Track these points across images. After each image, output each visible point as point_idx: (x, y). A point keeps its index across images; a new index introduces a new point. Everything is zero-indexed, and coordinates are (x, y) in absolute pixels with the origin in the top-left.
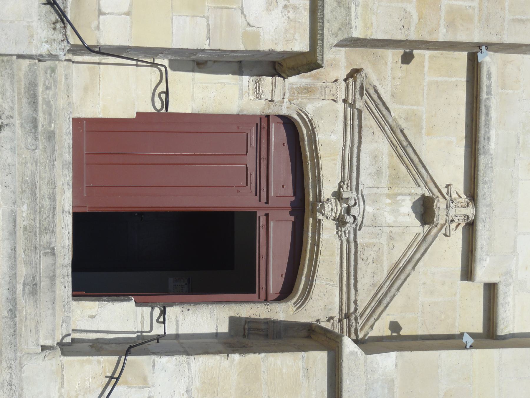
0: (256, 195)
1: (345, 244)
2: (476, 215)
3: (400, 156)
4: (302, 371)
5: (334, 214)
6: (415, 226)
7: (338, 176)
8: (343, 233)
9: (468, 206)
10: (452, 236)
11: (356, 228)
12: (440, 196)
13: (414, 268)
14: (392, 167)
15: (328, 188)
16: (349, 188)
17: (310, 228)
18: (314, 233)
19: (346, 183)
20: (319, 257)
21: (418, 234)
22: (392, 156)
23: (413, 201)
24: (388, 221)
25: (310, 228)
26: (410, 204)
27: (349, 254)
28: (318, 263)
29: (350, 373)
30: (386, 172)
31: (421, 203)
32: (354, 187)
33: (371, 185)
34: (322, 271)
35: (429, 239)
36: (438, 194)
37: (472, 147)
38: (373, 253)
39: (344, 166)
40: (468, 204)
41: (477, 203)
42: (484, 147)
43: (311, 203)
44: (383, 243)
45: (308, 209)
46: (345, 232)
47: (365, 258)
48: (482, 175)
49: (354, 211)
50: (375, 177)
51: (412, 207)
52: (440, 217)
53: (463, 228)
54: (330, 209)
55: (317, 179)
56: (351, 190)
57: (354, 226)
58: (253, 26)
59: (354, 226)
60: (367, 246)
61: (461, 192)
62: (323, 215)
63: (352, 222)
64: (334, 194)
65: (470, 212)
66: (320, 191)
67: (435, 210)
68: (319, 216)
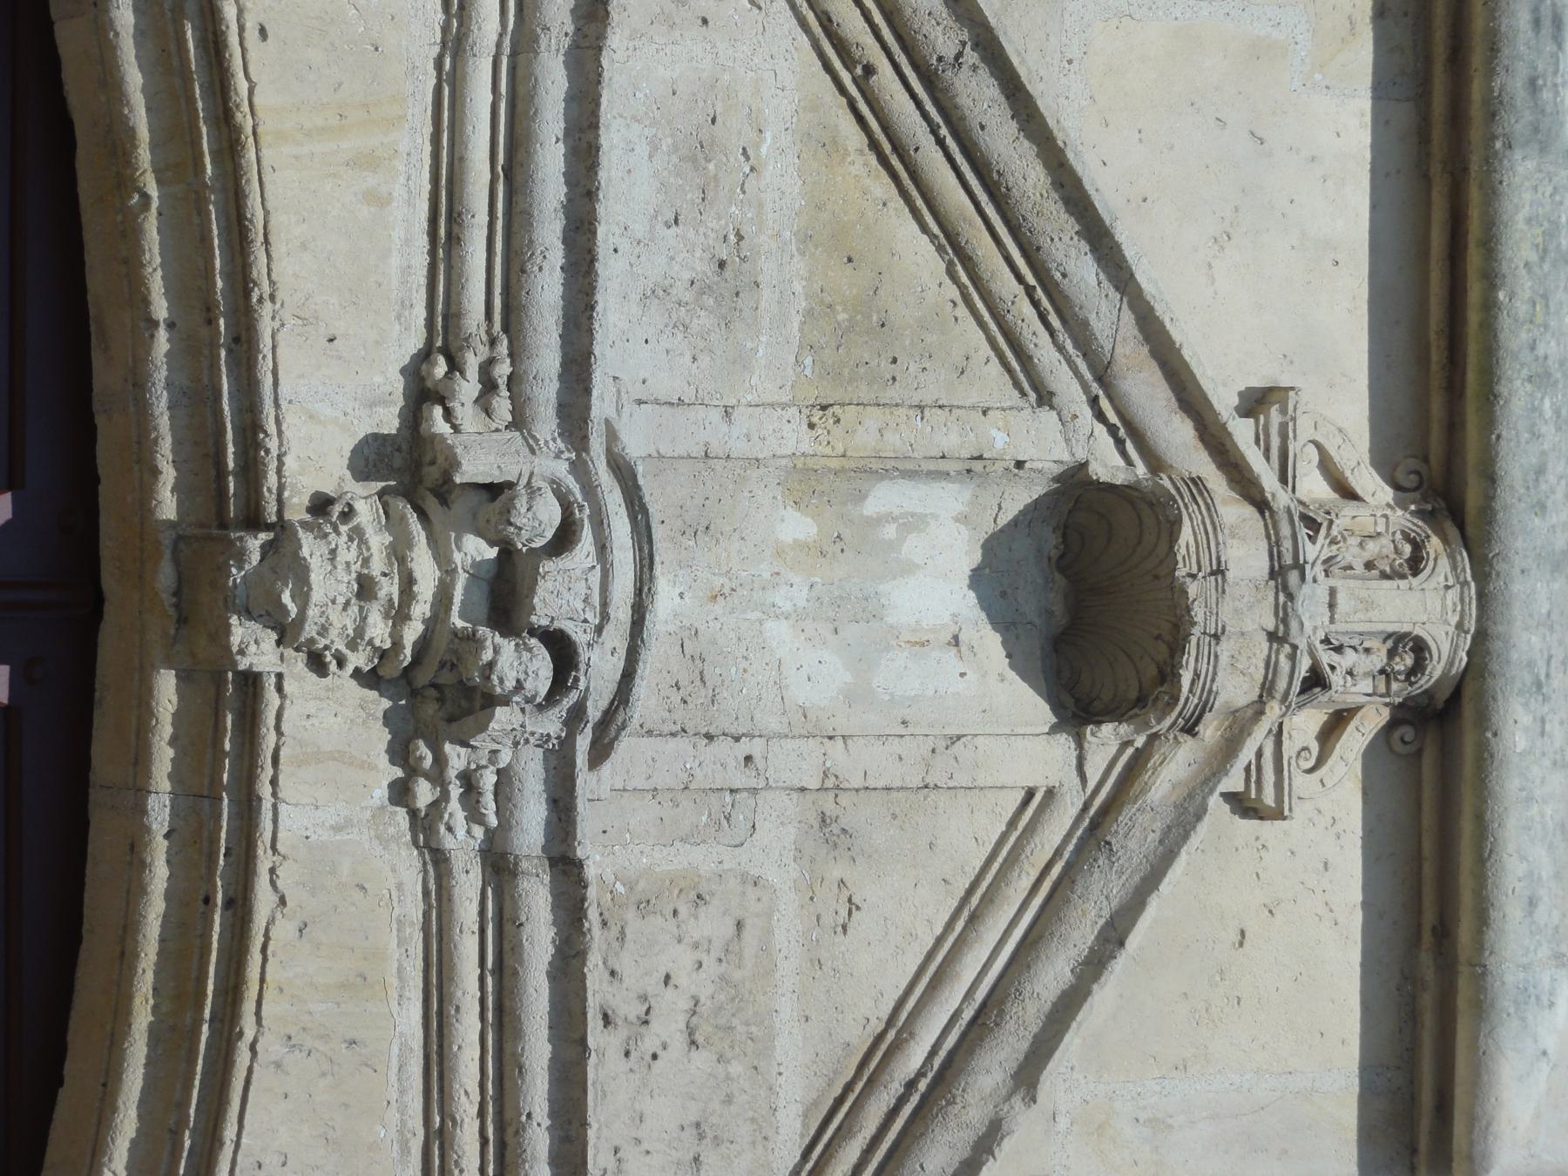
1: (468, 884)
2: (1482, 638)
3: (892, 153)
5: (379, 630)
6: (1017, 740)
7: (406, 305)
8: (455, 791)
9: (1415, 564)
10: (1300, 813)
11: (567, 744)
12: (1216, 482)
13: (1027, 1077)
14: (833, 241)
15: (323, 405)
16: (502, 405)
17: (163, 757)
18: (196, 795)
19: (472, 363)
20: (249, 1007)
21: (1036, 802)
22: (830, 146)
23: (988, 528)
24: (801, 692)
25: (163, 757)
26: (960, 552)
27: (503, 970)
28: (242, 1057)
30: (785, 277)
31: (1051, 541)
32: (546, 393)
33: (665, 386)
35: (1137, 833)
36: (1202, 465)
37: (1422, 97)
38: (687, 958)
39: (455, 218)
40: (1417, 546)
41: (1487, 538)
42: (1533, 85)
43: (167, 539)
44: (772, 875)
45: (134, 599)
46: (469, 781)
47: (630, 1010)
48: (1521, 308)
49: (560, 594)
50: (704, 320)
51: (977, 579)
52: (1225, 649)
53: (1369, 755)
54: (344, 585)
55: (227, 323)
56: (519, 422)
57: (551, 724)
59: (551, 724)
60: (644, 906)
62: (286, 633)
63: (543, 687)
64: (371, 458)
65: (1432, 607)
66: (250, 431)
67: (1193, 589)
68: (254, 646)
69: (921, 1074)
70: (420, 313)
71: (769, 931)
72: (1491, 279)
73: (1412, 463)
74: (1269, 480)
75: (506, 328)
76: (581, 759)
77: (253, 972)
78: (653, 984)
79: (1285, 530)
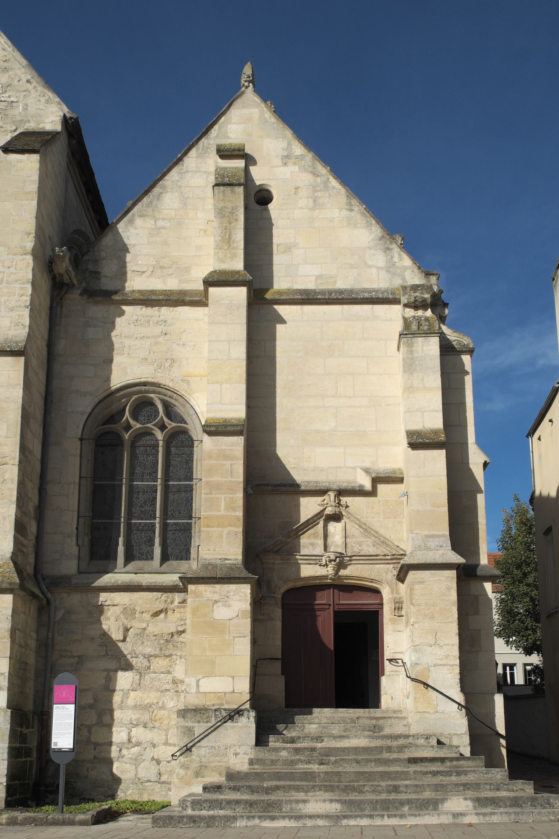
32: (320, 558)
34: (366, 575)
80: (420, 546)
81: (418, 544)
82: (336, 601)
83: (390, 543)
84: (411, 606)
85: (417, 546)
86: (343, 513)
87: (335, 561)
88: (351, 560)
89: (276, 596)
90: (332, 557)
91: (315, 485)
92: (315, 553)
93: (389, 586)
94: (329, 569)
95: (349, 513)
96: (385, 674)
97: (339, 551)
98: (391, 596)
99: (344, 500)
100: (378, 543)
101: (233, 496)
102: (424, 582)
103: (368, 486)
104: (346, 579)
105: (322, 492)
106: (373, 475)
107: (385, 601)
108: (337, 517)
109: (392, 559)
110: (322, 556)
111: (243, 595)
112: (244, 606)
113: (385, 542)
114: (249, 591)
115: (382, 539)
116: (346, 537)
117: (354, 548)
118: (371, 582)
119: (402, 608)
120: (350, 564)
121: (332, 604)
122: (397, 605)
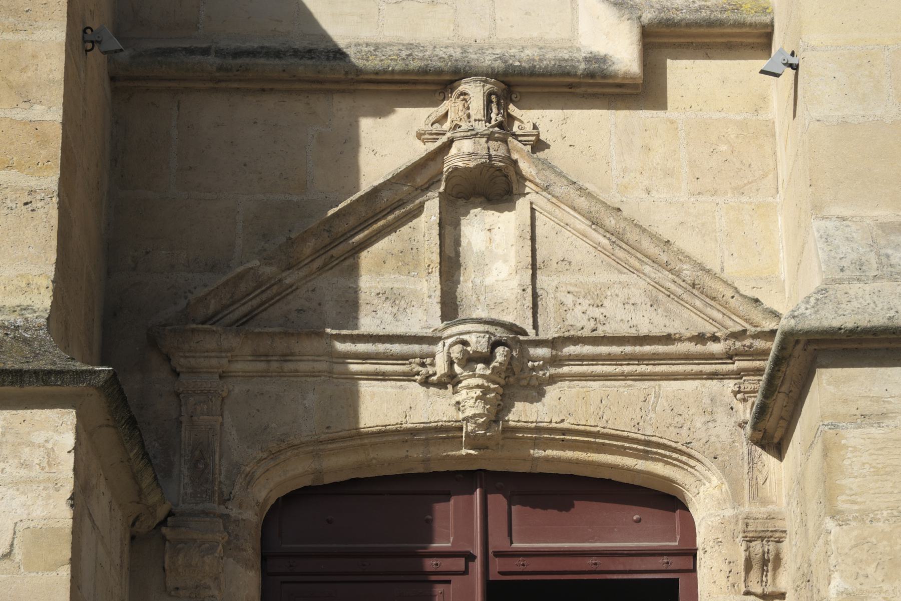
0: (449, 582)
4: (869, 430)
9: (465, 94)
29: (870, 310)
32: (425, 348)
34: (620, 421)
38: (579, 307)
39: (377, 374)
44: (555, 283)
47: (592, 324)
58: (12, 545)
61: (436, 112)
69: (609, 239)
70: (403, 383)
71: (571, 284)
72: (385, 72)
73: (437, 94)
74: (444, 139)
75: (408, 360)
76: (525, 338)
77: (583, 428)
78: (585, 317)
79: (458, 135)
80: (860, 265)
81: (854, 256)
82: (498, 542)
83: (720, 288)
84: (830, 524)
85: (844, 263)
86: (525, 167)
87: (487, 359)
88: (556, 361)
89: (234, 512)
90: (478, 343)
91: (404, 54)
92: (400, 329)
93: (723, 469)
94: (462, 395)
95: (547, 165)
96: (669, 104)
97: (509, 318)
98: (729, 512)
99: (527, 118)
100: (670, 294)
101: (21, 36)
102: (884, 415)
103: (624, 54)
104: (537, 443)
105: (430, 83)
106: (648, 16)
107: (703, 537)
108: (494, 186)
109: (730, 356)
110: (433, 340)
111: (36, 457)
112: (38, 512)
113: (700, 286)
114: (69, 439)
115: (688, 272)
116: (534, 267)
117: (568, 311)
118: (645, 456)
119: (778, 559)
120: (553, 380)
121: (478, 551)
122: (757, 547)
